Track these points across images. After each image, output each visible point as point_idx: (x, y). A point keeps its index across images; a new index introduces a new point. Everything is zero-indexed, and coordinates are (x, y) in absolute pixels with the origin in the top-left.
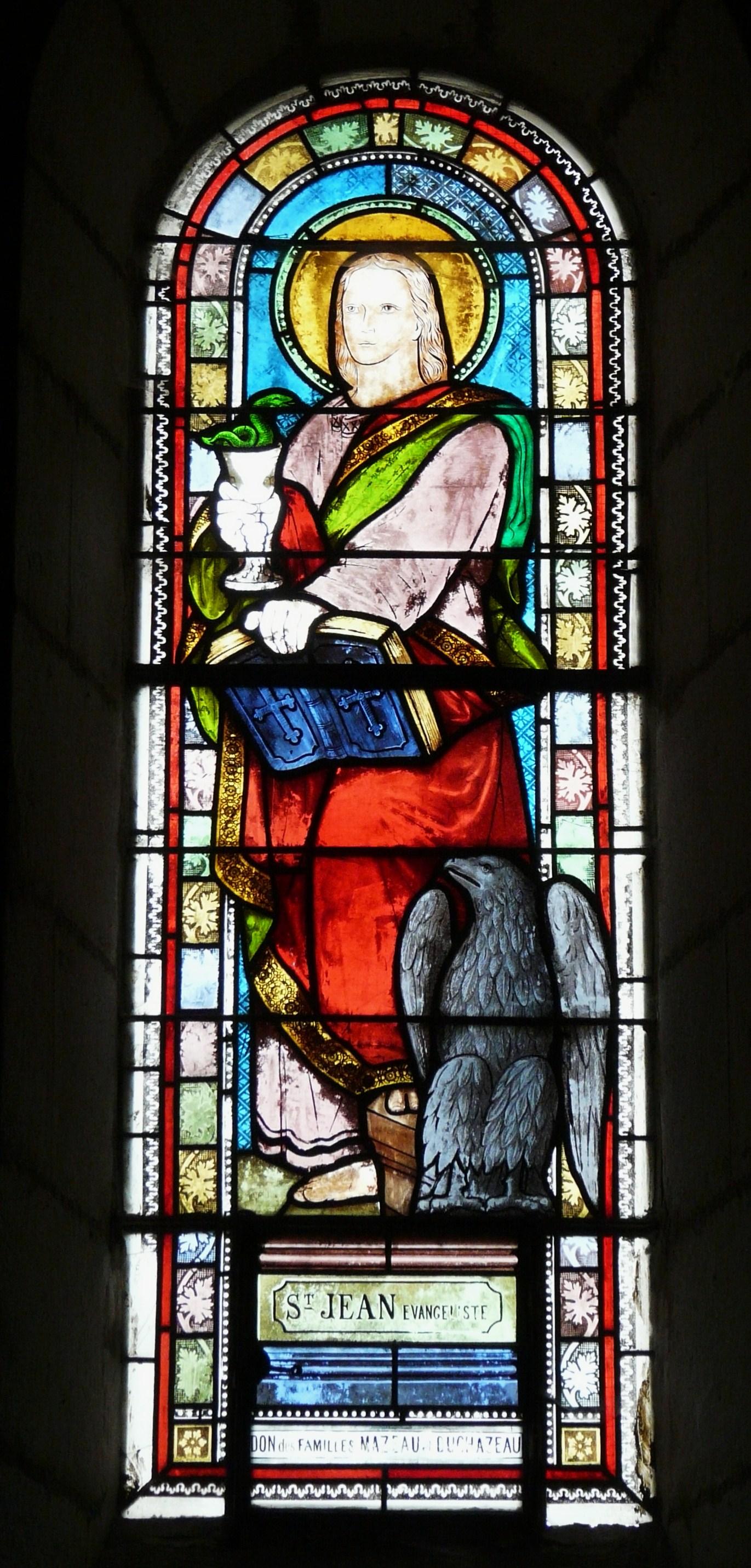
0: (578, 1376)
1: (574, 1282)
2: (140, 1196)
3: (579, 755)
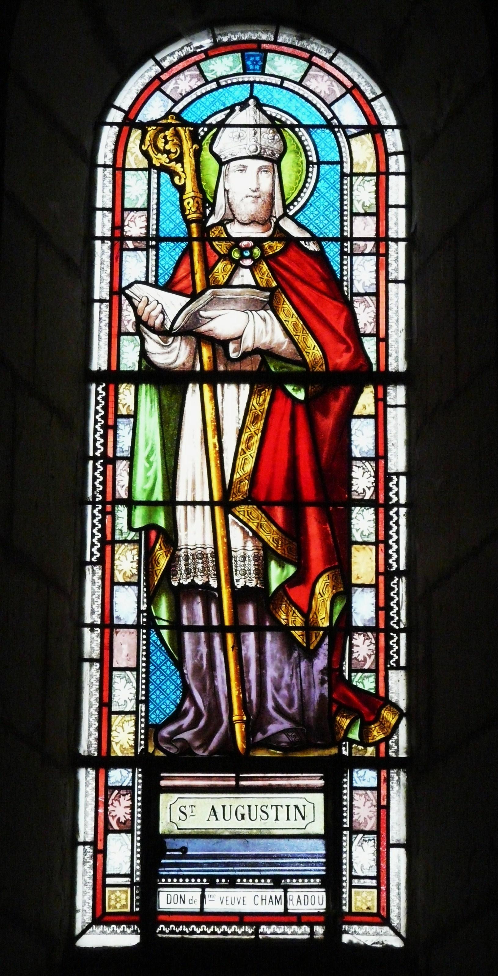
0: (362, 856)
1: (361, 795)
2: (88, 743)
3: (367, 464)
